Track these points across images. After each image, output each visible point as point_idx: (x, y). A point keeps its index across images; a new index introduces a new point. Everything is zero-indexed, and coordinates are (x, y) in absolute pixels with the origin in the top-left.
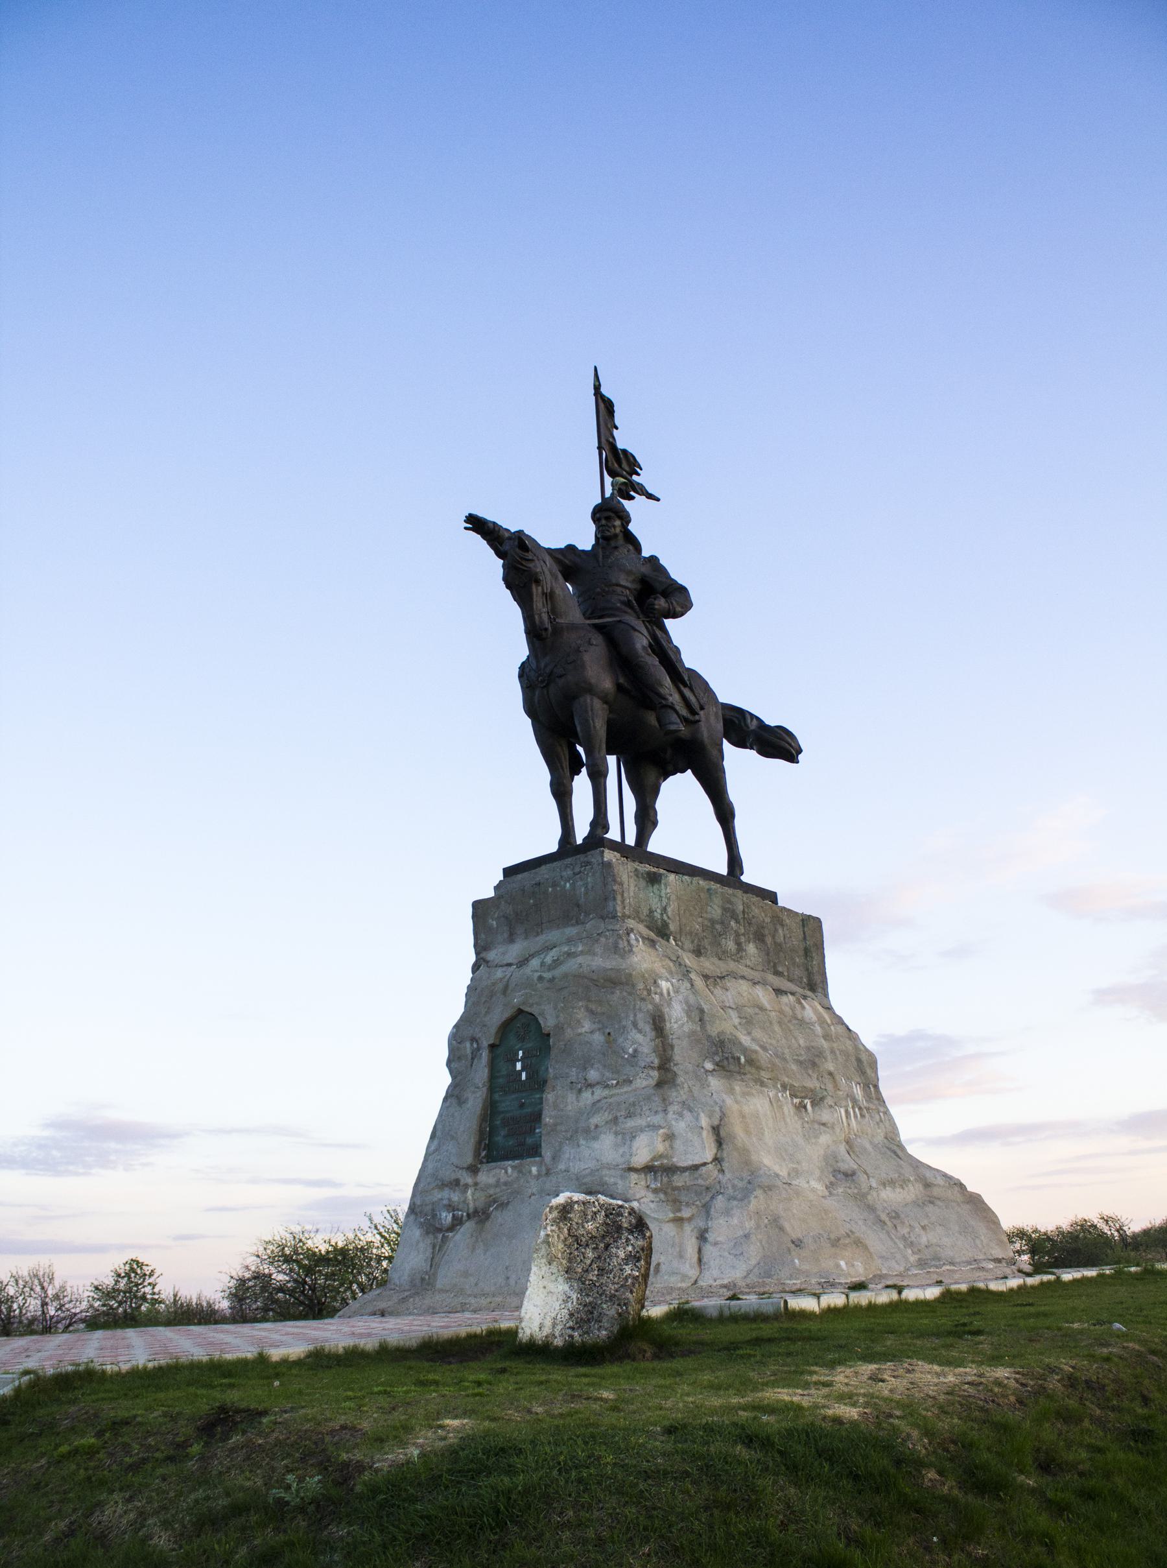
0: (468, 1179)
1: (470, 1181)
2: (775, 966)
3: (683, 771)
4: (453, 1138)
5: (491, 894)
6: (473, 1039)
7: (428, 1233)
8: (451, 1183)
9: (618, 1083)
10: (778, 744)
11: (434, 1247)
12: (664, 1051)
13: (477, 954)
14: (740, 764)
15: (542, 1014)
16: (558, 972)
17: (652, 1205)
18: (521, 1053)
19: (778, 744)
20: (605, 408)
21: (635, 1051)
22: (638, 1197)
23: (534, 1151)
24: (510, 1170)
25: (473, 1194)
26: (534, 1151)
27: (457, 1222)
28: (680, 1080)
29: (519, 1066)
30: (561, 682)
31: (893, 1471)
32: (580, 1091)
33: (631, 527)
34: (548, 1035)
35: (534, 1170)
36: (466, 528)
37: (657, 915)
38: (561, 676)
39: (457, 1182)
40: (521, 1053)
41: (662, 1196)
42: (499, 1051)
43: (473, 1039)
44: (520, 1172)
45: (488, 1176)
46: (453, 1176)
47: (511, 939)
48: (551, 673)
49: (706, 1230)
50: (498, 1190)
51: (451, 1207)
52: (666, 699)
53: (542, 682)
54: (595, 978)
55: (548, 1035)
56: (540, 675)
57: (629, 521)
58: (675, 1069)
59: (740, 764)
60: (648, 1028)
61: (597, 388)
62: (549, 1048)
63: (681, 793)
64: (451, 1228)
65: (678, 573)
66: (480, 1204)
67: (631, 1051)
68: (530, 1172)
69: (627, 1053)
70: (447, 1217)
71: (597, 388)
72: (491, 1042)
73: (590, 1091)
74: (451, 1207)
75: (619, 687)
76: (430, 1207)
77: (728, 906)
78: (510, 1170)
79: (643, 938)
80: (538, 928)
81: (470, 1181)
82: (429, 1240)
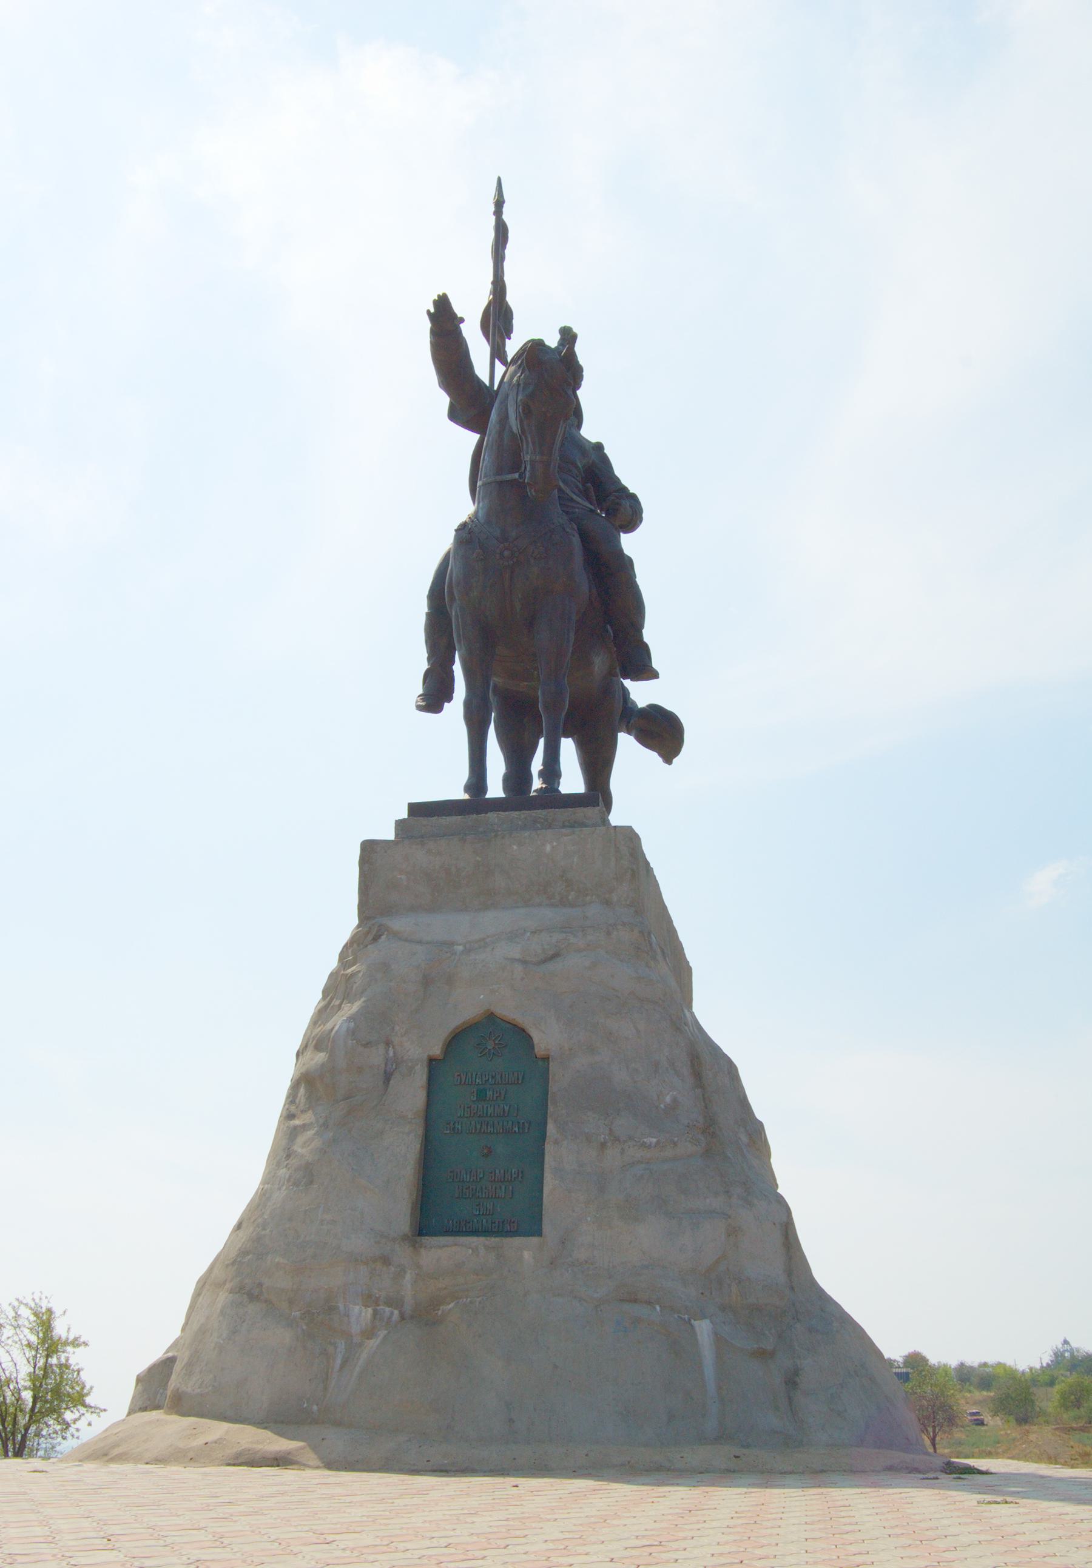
0: (402, 1254)
14: (627, 744)
32: (603, 1145)
59: (627, 744)
78: (482, 1251)
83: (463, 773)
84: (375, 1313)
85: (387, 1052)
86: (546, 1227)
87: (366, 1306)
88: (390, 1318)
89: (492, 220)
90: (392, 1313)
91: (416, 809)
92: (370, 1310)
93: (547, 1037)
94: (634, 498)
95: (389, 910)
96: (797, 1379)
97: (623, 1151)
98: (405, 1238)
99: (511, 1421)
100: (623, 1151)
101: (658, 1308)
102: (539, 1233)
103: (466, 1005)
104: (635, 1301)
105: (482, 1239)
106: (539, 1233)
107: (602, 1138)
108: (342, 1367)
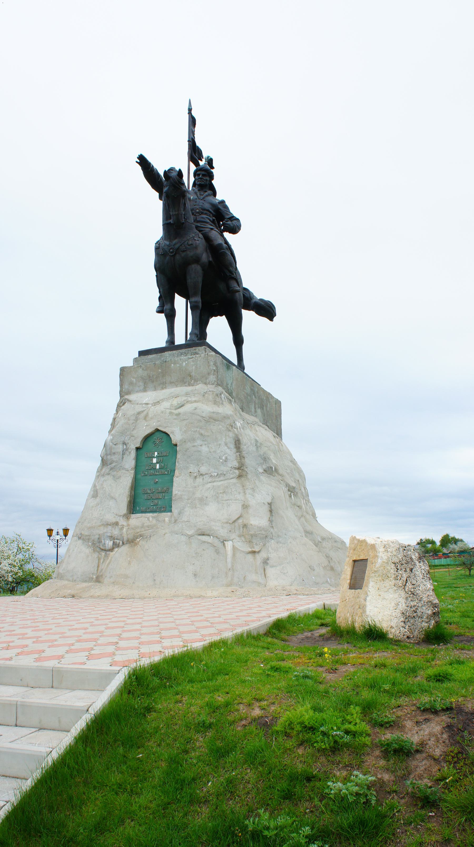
0: (122, 522)
1: (125, 524)
2: (266, 423)
3: (221, 315)
4: (112, 498)
5: (131, 364)
6: (124, 443)
7: (94, 551)
8: (113, 524)
9: (217, 475)
10: (266, 310)
11: (99, 559)
12: (241, 459)
13: (121, 396)
14: (248, 317)
15: (173, 433)
16: (181, 410)
17: (239, 544)
18: (156, 454)
19: (266, 310)
20: (193, 122)
21: (226, 458)
22: (231, 539)
23: (167, 508)
24: (151, 519)
25: (127, 531)
26: (167, 508)
27: (116, 545)
28: (249, 476)
29: (155, 461)
30: (183, 254)
31: (202, 671)
32: (196, 477)
33: (213, 182)
34: (176, 445)
35: (167, 519)
36: (137, 162)
37: (229, 386)
38: (184, 251)
39: (117, 524)
40: (156, 454)
41: (243, 538)
42: (141, 451)
43: (124, 443)
44: (157, 520)
45: (138, 520)
46: (114, 520)
47: (145, 390)
48: (178, 249)
49: (268, 559)
50: (143, 530)
51: (111, 538)
52: (233, 274)
53: (172, 252)
54: (204, 416)
55: (176, 445)
56: (171, 249)
57: (213, 179)
58: (246, 470)
59: (248, 317)
60: (232, 446)
61: (190, 110)
62: (176, 452)
63: (218, 327)
64: (112, 550)
65: (234, 210)
66: (131, 537)
67: (224, 458)
68: (164, 520)
69: (222, 459)
70: (109, 544)
71: (190, 110)
72: (138, 445)
73: (202, 477)
74: (111, 538)
75: (210, 262)
76: (97, 536)
77: (252, 388)
78: (151, 519)
79: (227, 398)
80: (163, 385)
81: (125, 524)
82: (96, 555)
83: (165, 336)
84: (114, 542)
85: (123, 447)
86: (173, 509)
87: (111, 541)
88: (119, 544)
89: (187, 116)
90: (119, 543)
91: (142, 353)
92: (112, 542)
93: (176, 437)
94: (157, 249)
95: (129, 393)
96: (268, 562)
97: (203, 479)
98: (124, 516)
99: (155, 580)
100: (203, 479)
101: (212, 537)
102: (171, 511)
103: (144, 429)
104: (203, 535)
105: (151, 514)
106: (171, 511)
107: (195, 475)
108: (103, 562)
